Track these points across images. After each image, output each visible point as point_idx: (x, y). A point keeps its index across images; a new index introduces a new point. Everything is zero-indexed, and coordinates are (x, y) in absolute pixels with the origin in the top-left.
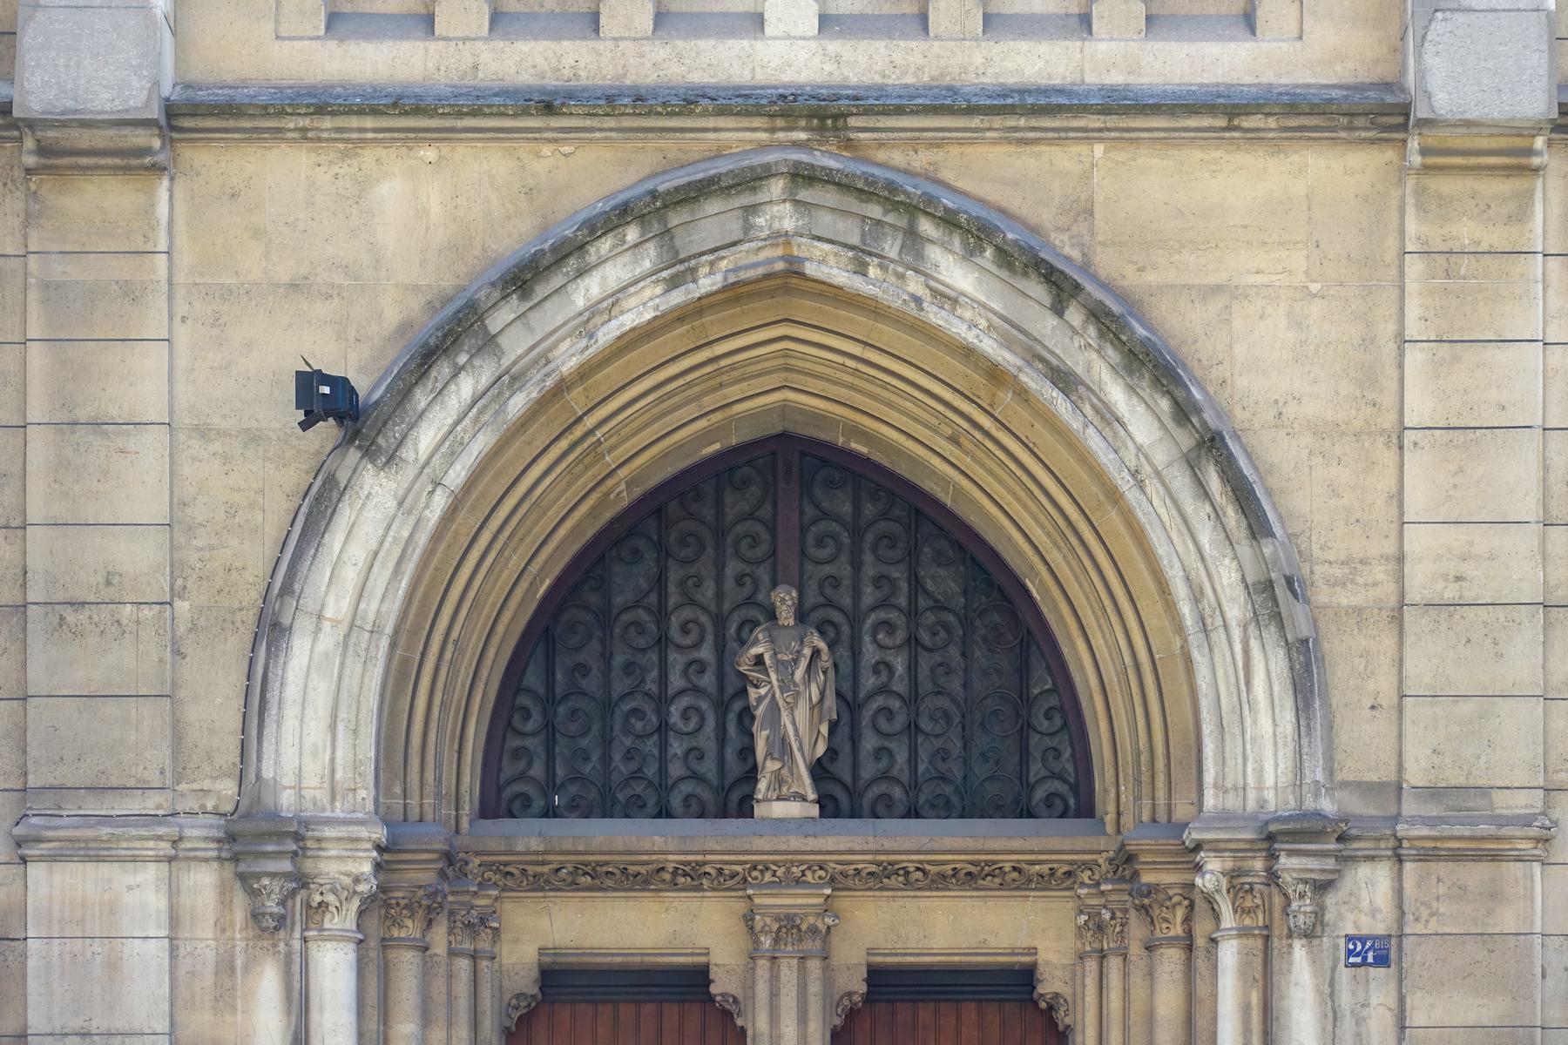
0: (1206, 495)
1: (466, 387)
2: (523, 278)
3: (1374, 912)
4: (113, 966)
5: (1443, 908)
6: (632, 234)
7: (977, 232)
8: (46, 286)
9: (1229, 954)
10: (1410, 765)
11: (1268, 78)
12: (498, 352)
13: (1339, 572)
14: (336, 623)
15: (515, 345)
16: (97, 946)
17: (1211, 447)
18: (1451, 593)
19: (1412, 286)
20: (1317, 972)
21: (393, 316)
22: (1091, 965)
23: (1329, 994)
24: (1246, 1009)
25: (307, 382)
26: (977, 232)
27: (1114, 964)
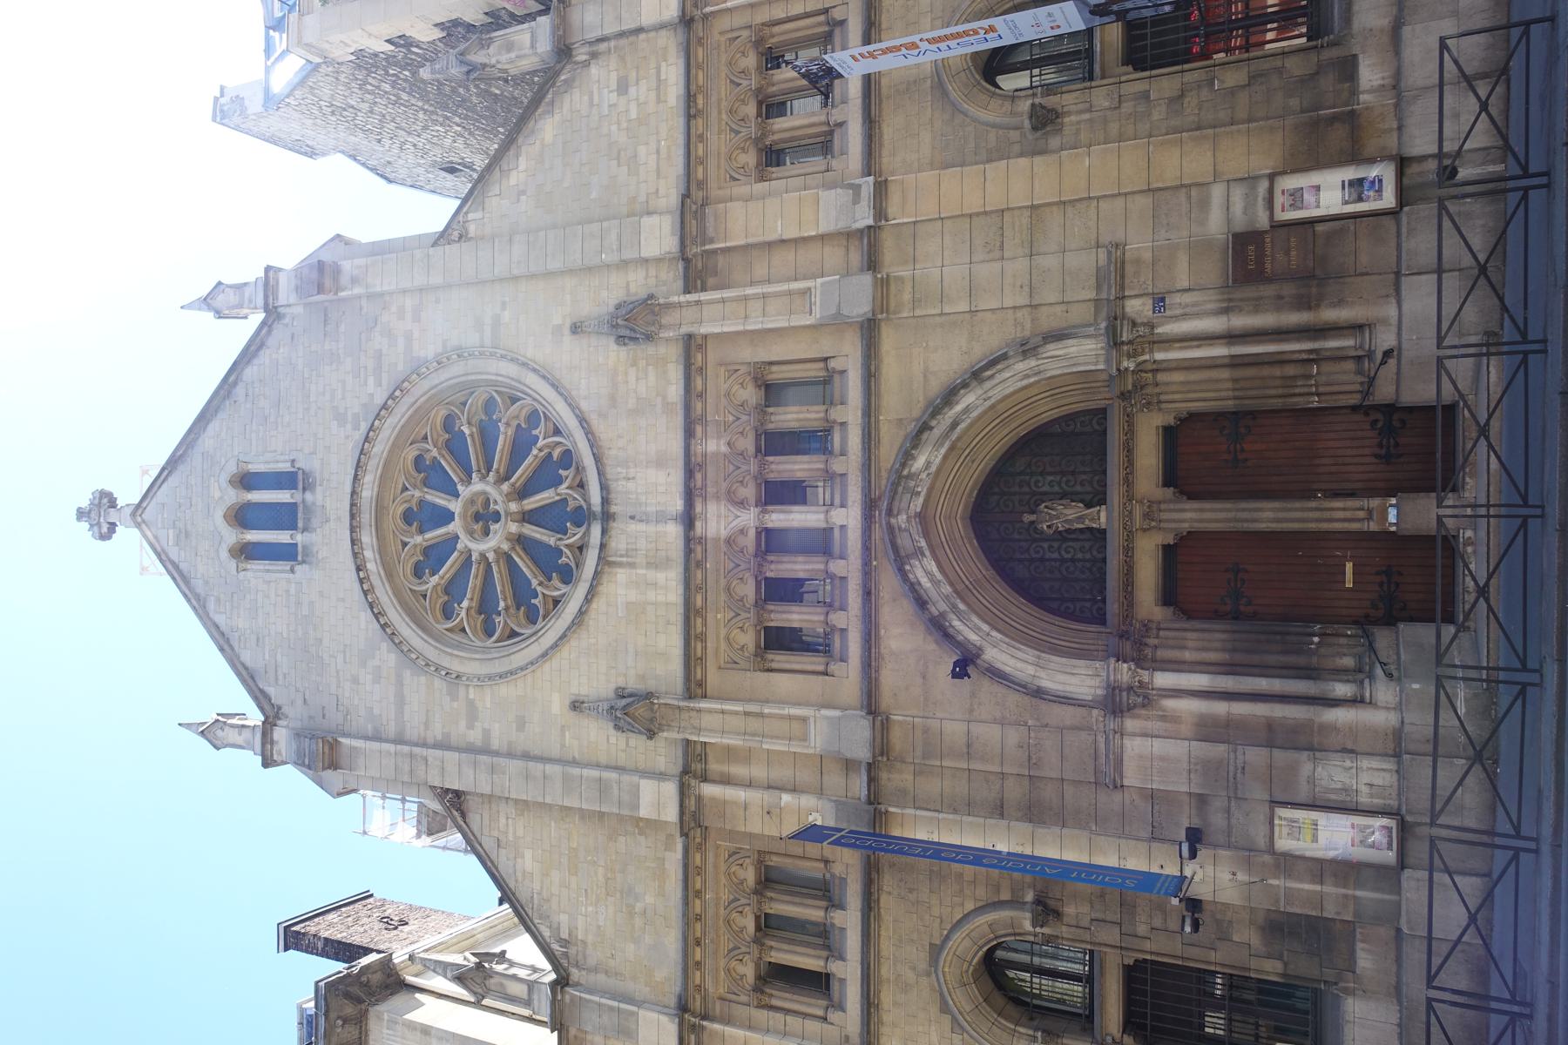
1: (956, 623)
2: (921, 603)
4: (1162, 759)
15: (943, 606)
17: (976, 375)
18: (1027, 289)
21: (933, 646)
23: (1176, 318)
26: (907, 456)
27: (1163, 398)
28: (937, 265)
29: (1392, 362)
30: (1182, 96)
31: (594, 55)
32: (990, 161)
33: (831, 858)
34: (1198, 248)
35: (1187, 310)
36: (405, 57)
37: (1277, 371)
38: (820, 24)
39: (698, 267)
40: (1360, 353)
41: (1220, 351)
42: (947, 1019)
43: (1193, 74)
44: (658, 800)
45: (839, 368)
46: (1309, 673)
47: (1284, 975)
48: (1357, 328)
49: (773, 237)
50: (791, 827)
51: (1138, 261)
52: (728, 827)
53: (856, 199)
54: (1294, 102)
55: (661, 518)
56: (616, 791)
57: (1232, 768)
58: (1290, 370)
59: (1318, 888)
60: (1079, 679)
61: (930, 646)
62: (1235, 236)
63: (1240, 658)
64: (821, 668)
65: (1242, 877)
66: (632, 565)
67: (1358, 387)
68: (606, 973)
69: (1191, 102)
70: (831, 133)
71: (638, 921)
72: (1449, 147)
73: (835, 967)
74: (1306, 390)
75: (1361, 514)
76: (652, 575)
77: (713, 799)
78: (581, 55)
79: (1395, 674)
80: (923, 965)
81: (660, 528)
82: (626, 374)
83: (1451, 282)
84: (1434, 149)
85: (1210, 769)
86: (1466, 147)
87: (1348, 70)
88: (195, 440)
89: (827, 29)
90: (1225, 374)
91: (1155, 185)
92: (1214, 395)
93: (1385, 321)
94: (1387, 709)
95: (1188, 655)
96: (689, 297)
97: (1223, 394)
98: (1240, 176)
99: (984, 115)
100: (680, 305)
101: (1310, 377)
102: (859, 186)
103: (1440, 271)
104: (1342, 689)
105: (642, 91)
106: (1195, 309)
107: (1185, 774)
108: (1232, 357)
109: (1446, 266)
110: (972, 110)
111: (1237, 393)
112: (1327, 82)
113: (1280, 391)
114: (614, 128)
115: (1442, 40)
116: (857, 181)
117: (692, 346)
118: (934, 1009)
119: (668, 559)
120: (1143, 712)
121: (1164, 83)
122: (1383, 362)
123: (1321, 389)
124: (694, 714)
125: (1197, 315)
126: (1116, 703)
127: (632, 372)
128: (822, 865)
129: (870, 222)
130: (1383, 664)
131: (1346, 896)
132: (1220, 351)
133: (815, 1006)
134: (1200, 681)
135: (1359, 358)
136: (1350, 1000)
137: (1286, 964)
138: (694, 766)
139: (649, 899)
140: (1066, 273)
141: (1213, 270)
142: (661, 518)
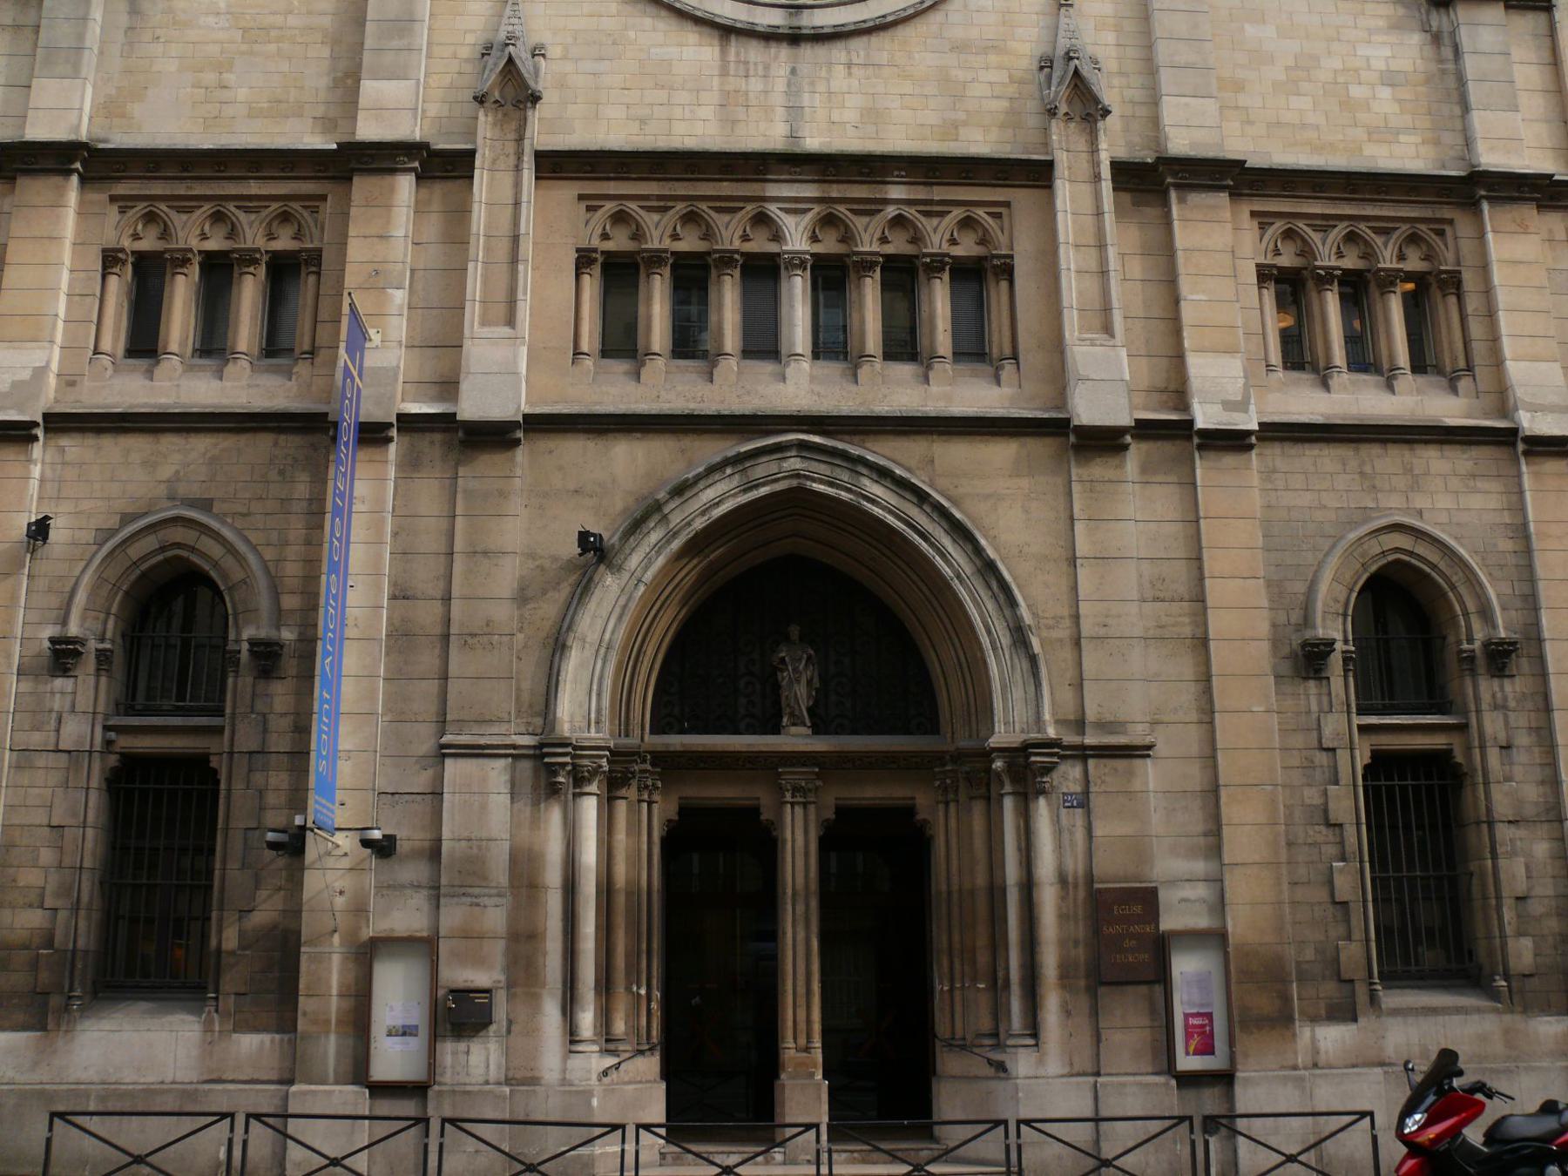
0: (990, 588)
1: (654, 537)
2: (681, 490)
3: (1500, 706)
4: (484, 807)
5: (1107, 779)
6: (729, 471)
7: (883, 474)
8: (465, 491)
9: (1008, 804)
10: (1088, 711)
11: (982, 446)
12: (668, 523)
13: (1051, 622)
14: (591, 644)
15: (675, 519)
16: (476, 797)
17: (988, 569)
18: (1102, 632)
19: (1075, 496)
20: (1051, 811)
21: (619, 505)
22: (941, 807)
23: (1056, 821)
24: (1018, 828)
25: (583, 536)
26: (883, 474)
27: (952, 806)
28: (1133, 509)
29: (990, 1071)
30: (1329, 825)
31: (1436, 39)
32: (1269, 584)
33: (318, 360)
34: (1139, 848)
35: (1066, 835)
37: (982, 941)
38: (1454, 359)
39: (1150, 181)
40: (1002, 1036)
41: (1012, 873)
42: (114, 522)
43: (1356, 836)
44: (393, 109)
45: (1004, 375)
46: (605, 985)
47: (219, 951)
48: (1034, 1030)
49: (1185, 286)
50: (364, 304)
51: (1131, 774)
52: (353, 211)
53: (1229, 406)
54: (1309, 954)
55: (795, 112)
56: (395, 43)
57: (476, 891)
58: (983, 958)
59: (334, 992)
60: (583, 707)
61: (619, 503)
62: (1153, 892)
63: (620, 901)
64: (585, 347)
65: (340, 902)
66: (724, 73)
67: (959, 1034)
68: (131, 28)
69: (1322, 833)
70: (1315, 370)
71: (210, 77)
72: (1241, 1124)
73: (170, 366)
74: (957, 975)
75: (802, 1041)
76: (711, 97)
79: (605, 1080)
80: (182, 490)
81: (780, 113)
82: (1000, 67)
83: (1080, 1134)
84: (1241, 1108)
85: (473, 871)
86: (1241, 1139)
87: (1344, 1012)
90: (981, 880)
91: (1223, 793)
92: (952, 864)
93: (1041, 1062)
94: (564, 1071)
95: (621, 837)
96: (1106, 172)
97: (955, 880)
98: (1227, 896)
99: (1327, 575)
100: (1094, 150)
101: (975, 980)
102: (1246, 411)
103: (1097, 1120)
104: (587, 1020)
105: (1385, 102)
106: (1066, 842)
107: (466, 834)
108: (1004, 890)
109: (1104, 1126)
110: (1334, 561)
111: (955, 896)
112: (1330, 989)
113: (957, 946)
114: (1338, 64)
115: (1371, 1114)
116: (1252, 408)
117: (1038, 174)
118: (122, 505)
119: (735, 122)
120: (543, 784)
121: (1347, 803)
122: (990, 1062)
123: (957, 994)
124: (512, 160)
125: (1059, 847)
127: (1003, 76)
128: (306, 347)
129: (1200, 424)
130: (617, 1066)
131: (328, 1022)
132: (1012, 873)
133: (114, 336)
134: (589, 855)
135: (996, 1035)
136: (197, 1027)
137: (232, 953)
138: (444, 167)
139: (242, 94)
140: (1133, 687)
141: (1112, 867)
142: (795, 112)
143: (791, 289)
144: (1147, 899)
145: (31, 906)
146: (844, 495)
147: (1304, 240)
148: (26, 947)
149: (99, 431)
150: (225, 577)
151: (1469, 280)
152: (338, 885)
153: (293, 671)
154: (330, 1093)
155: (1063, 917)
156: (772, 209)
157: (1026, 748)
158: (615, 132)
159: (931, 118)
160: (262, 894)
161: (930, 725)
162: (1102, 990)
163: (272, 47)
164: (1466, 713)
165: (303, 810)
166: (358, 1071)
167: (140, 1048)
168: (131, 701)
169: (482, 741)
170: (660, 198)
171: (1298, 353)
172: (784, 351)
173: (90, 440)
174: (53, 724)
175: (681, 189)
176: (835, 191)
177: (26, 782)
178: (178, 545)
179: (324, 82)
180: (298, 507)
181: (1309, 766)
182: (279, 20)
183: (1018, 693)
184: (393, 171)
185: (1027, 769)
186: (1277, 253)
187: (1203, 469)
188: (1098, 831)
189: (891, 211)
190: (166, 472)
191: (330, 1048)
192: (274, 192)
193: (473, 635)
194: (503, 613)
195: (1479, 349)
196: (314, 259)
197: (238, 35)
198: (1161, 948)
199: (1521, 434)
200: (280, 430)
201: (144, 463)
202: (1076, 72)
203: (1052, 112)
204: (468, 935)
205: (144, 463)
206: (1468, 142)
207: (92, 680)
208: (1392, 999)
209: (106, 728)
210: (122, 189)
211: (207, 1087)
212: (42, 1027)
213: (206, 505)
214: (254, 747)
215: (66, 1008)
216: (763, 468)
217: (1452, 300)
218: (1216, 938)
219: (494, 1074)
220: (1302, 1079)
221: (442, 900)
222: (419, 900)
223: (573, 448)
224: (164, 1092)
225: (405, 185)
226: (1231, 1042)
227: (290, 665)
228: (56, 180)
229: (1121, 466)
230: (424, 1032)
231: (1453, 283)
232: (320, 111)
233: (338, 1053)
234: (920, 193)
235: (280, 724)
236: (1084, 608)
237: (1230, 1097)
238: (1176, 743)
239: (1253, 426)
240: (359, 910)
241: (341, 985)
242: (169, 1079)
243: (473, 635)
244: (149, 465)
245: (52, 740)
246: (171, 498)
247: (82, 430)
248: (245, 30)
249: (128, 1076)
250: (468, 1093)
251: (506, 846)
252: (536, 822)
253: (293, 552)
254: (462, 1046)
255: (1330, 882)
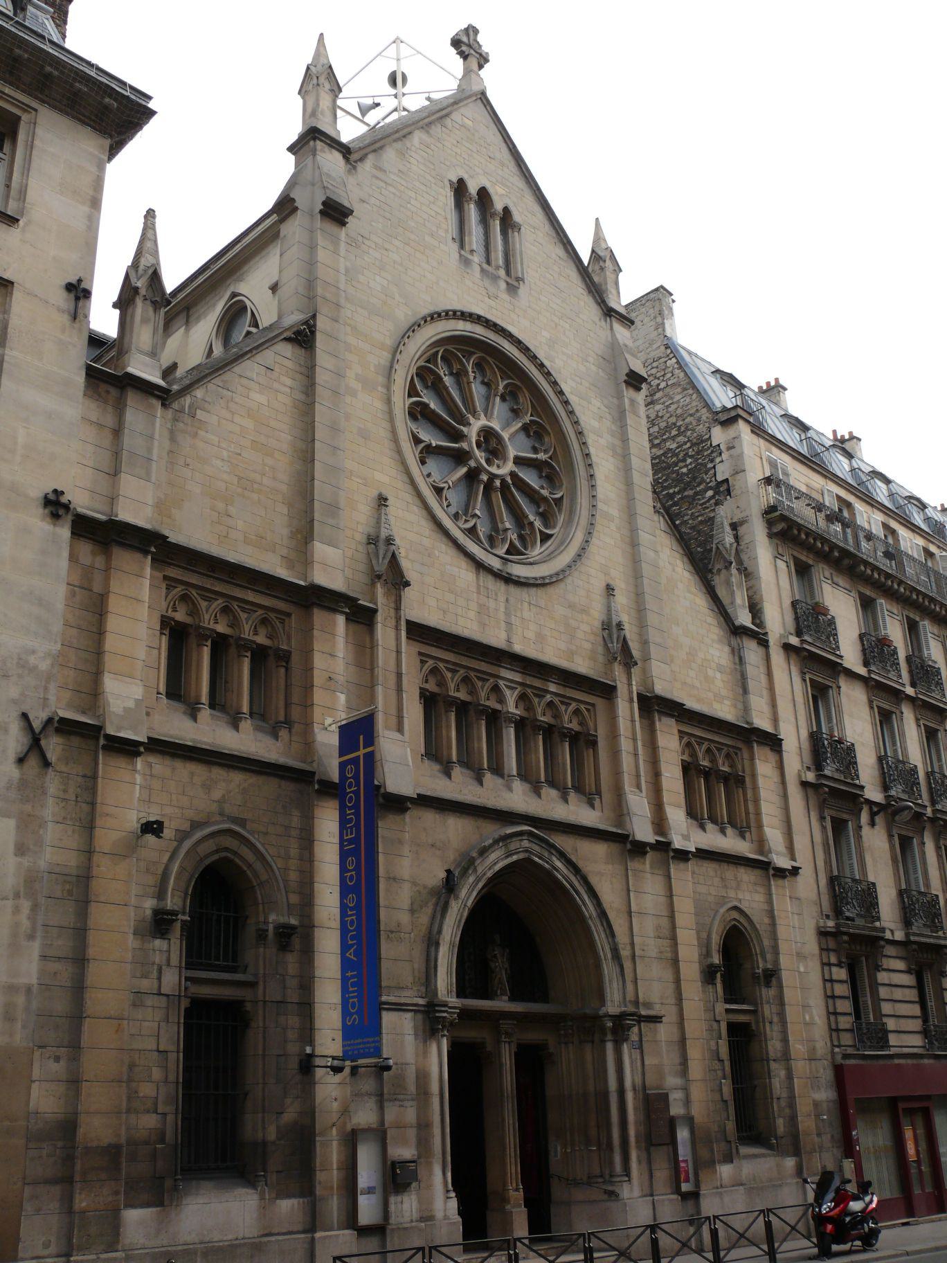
1: (471, 879)
7: (562, 855)
9: (610, 1046)
15: (480, 870)
28: (648, 887)
29: (606, 1197)
36: (703, 481)
39: (654, 706)
42: (186, 826)
62: (667, 1095)
71: (220, 506)
76: (473, 606)
77: (335, 624)
78: (734, 642)
80: (228, 809)
81: (503, 624)
87: (728, 1159)
88: (531, 187)
89: (445, 758)
96: (635, 699)
122: (606, 1192)
124: (393, 622)
126: (768, 1002)
131: (332, 1188)
132: (612, 1084)
136: (256, 1197)
137: (273, 1143)
143: (508, 734)
144: (664, 1098)
145: (148, 1112)
146: (547, 866)
147: (235, 617)
148: (147, 1143)
149: (174, 756)
150: (256, 875)
151: (295, 659)
152: (334, 1094)
153: (297, 947)
154: (337, 1236)
155: (635, 1109)
156: (501, 683)
157: (623, 1016)
158: (431, 617)
159: (563, 646)
160: (288, 1101)
161: (545, 999)
162: (652, 1149)
163: (255, 496)
164: (755, 1004)
165: (311, 1042)
166: (351, 1220)
167: (221, 1213)
168: (195, 957)
169: (403, 1001)
170: (455, 664)
171: (176, 688)
172: (506, 772)
173: (168, 761)
174: (155, 974)
175: (465, 661)
176: (529, 681)
177: (140, 1017)
178: (227, 849)
179: (285, 532)
180: (294, 833)
181: (710, 1030)
182: (258, 477)
183: (615, 985)
184: (335, 611)
185: (621, 1026)
186: (175, 610)
187: (675, 869)
188: (646, 1063)
189: (548, 697)
190: (217, 794)
191: (334, 1206)
192: (263, 603)
193: (392, 932)
194: (405, 918)
195: (296, 713)
196: (284, 657)
197: (235, 480)
198: (672, 1123)
199: (382, 790)
200: (282, 777)
201: (203, 785)
202: (394, 555)
203: (379, 577)
204: (400, 1126)
205: (203, 785)
206: (112, 500)
207: (178, 942)
208: (744, 1150)
209: (187, 979)
210: (173, 572)
211: (265, 1239)
212: (160, 1204)
213: (242, 822)
214: (279, 999)
215: (175, 1188)
216: (514, 844)
217: (282, 670)
218: (690, 1120)
219: (415, 1216)
220: (721, 1193)
221: (386, 1104)
222: (371, 1104)
223: (429, 817)
224: (240, 1245)
225: (341, 620)
226: (696, 1175)
227: (296, 942)
228: (138, 556)
229: (644, 863)
230: (379, 1191)
231: (284, 657)
232: (284, 552)
233: (339, 1208)
234: (561, 691)
235: (292, 983)
236: (636, 939)
237: (698, 1205)
238: (670, 1015)
239: (142, 738)
240: (345, 1112)
241: (338, 1161)
242: (241, 1236)
243: (392, 932)
244: (207, 788)
245: (156, 986)
246: (221, 814)
247: (163, 753)
248: (240, 478)
249: (216, 1237)
250: (406, 1229)
251: (413, 1067)
252: (425, 1053)
253: (293, 864)
254: (399, 1198)
255: (721, 1090)
